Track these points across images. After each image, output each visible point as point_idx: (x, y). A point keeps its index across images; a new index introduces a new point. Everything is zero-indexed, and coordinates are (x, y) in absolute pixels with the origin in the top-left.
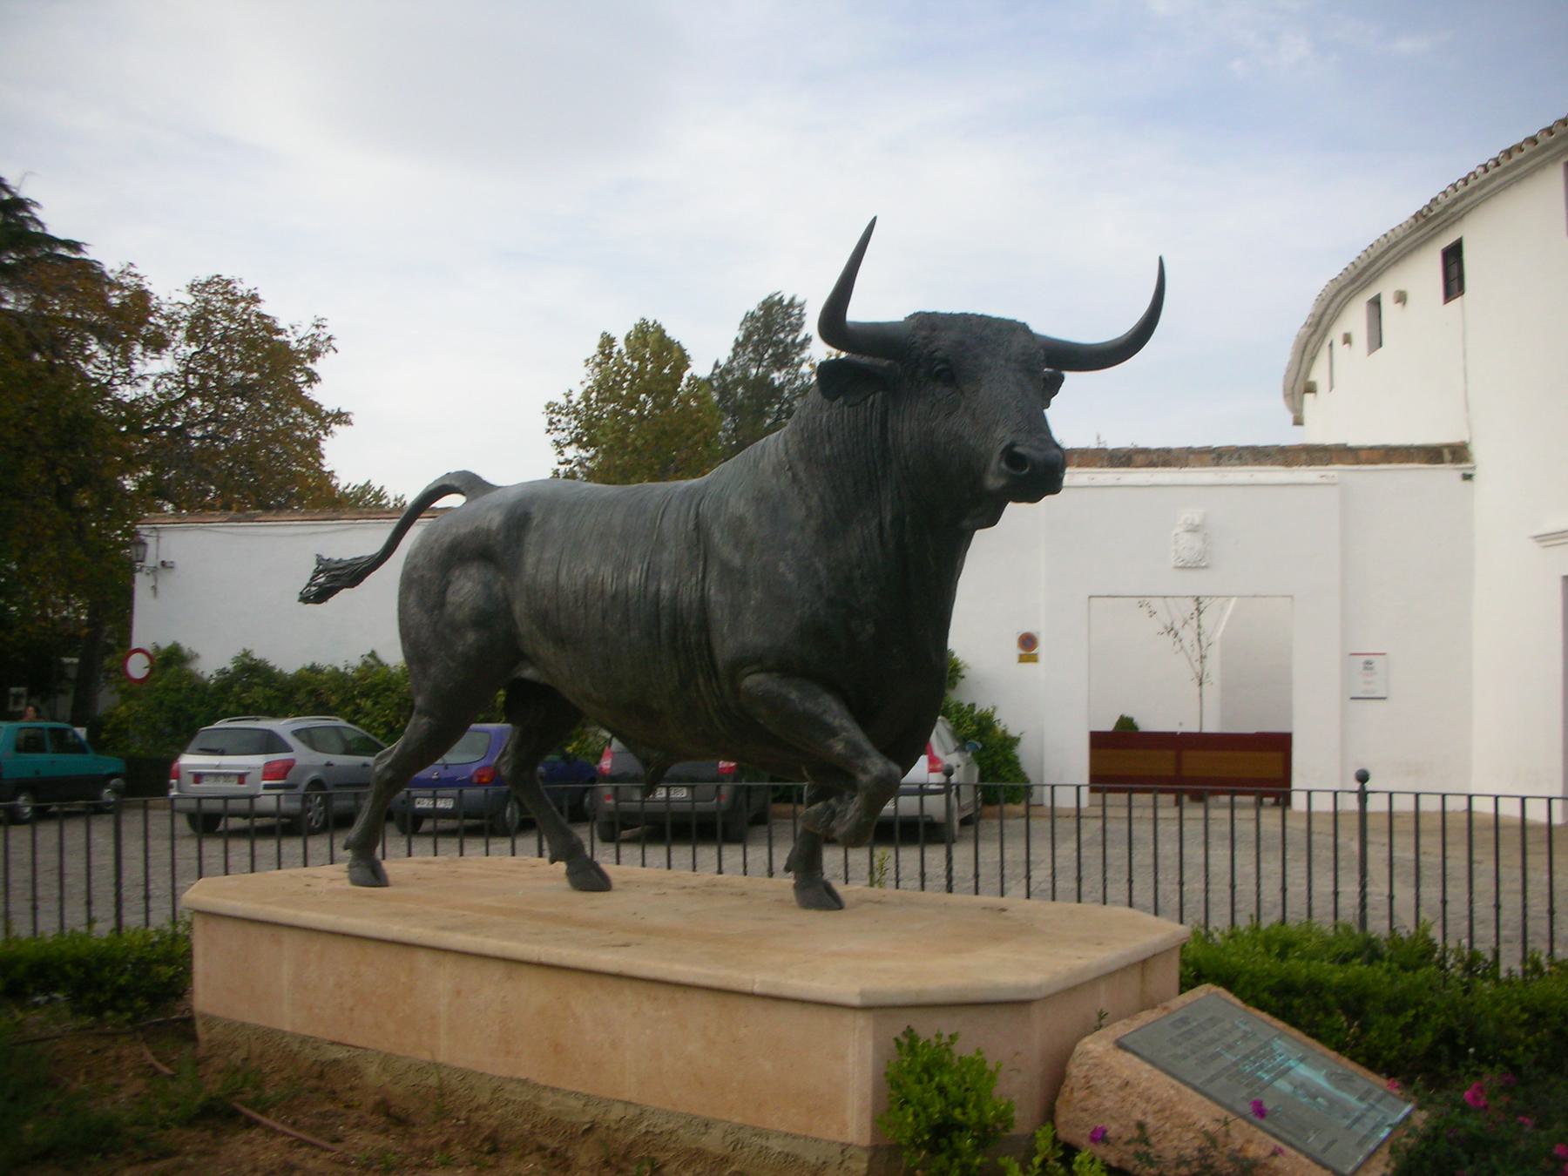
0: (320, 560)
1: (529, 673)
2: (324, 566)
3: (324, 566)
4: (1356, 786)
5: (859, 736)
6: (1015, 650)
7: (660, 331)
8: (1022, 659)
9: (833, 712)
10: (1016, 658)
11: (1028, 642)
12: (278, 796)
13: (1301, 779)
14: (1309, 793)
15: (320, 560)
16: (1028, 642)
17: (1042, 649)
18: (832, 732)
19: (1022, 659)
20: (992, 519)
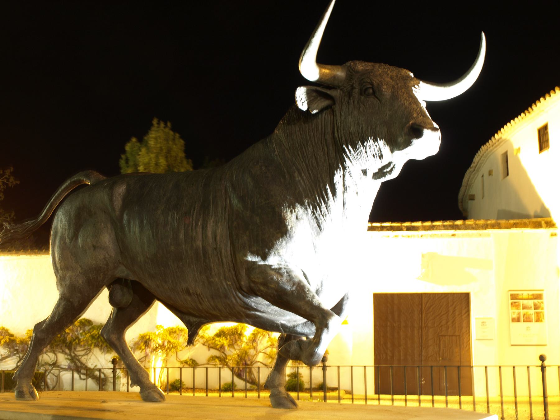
4: (540, 363)
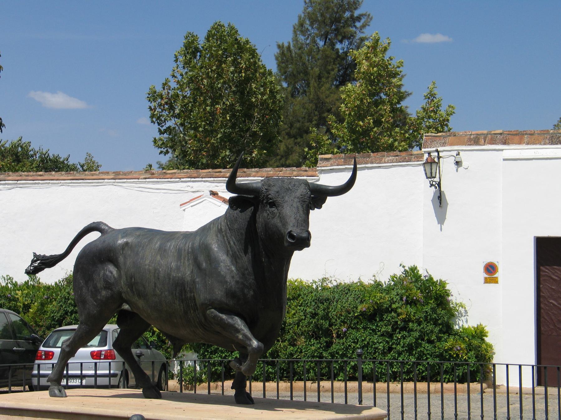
0: (35, 255)
1: (126, 307)
2: (37, 257)
3: (37, 257)
5: (249, 334)
6: (483, 275)
7: (233, 32)
8: (487, 281)
9: (239, 323)
10: (483, 280)
11: (491, 269)
12: (110, 363)
13: (499, 357)
14: (507, 365)
15: (35, 255)
16: (491, 269)
17: (500, 274)
18: (238, 331)
19: (487, 281)
20: (44, 256)
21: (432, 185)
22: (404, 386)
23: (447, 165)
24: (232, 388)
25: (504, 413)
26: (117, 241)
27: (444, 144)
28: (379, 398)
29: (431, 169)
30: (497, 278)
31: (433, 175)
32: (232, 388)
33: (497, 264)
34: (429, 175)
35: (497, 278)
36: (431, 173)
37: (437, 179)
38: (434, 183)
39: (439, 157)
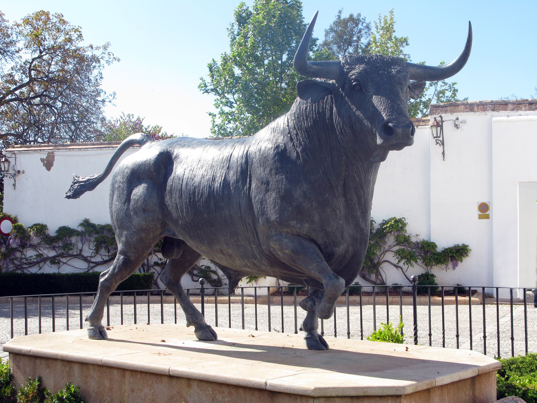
6: (477, 212)
8: (480, 217)
10: (477, 217)
11: (484, 208)
16: (484, 208)
19: (480, 217)
21: (437, 143)
22: (69, 299)
23: (448, 127)
24: (188, 326)
25: (370, 314)
26: (148, 189)
27: (446, 112)
28: (391, 316)
29: (437, 130)
30: (488, 214)
31: (439, 135)
32: (188, 326)
33: (479, 204)
34: (435, 135)
35: (488, 214)
36: (437, 133)
37: (441, 139)
38: (439, 142)
39: (442, 122)
